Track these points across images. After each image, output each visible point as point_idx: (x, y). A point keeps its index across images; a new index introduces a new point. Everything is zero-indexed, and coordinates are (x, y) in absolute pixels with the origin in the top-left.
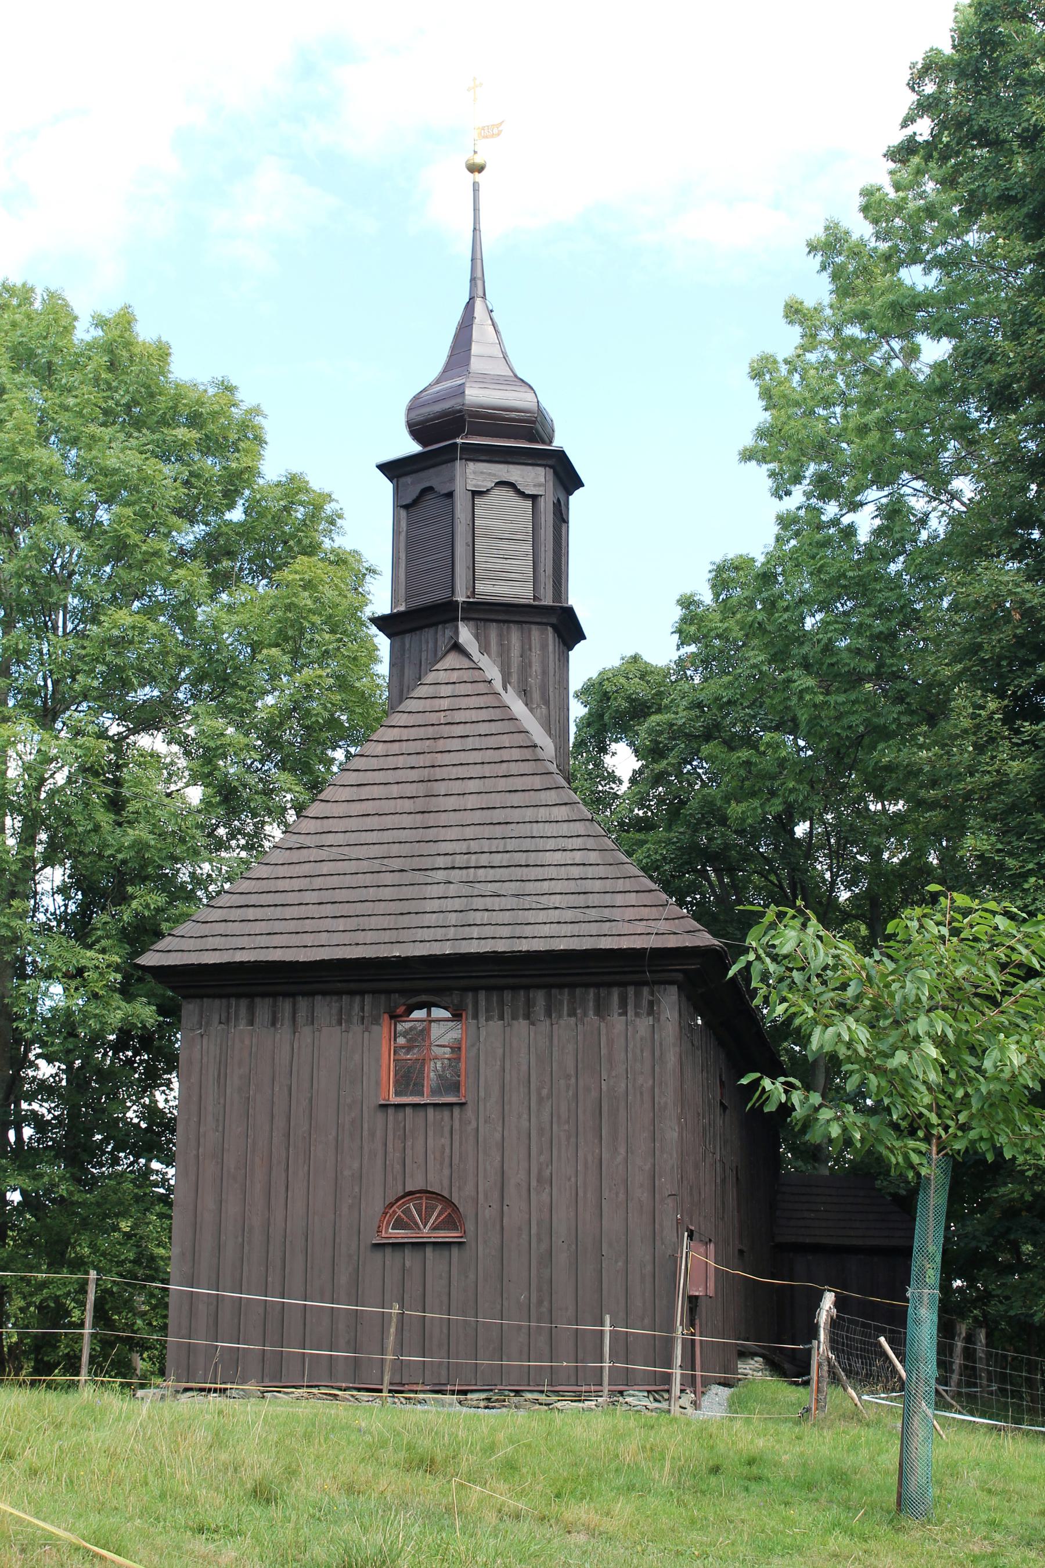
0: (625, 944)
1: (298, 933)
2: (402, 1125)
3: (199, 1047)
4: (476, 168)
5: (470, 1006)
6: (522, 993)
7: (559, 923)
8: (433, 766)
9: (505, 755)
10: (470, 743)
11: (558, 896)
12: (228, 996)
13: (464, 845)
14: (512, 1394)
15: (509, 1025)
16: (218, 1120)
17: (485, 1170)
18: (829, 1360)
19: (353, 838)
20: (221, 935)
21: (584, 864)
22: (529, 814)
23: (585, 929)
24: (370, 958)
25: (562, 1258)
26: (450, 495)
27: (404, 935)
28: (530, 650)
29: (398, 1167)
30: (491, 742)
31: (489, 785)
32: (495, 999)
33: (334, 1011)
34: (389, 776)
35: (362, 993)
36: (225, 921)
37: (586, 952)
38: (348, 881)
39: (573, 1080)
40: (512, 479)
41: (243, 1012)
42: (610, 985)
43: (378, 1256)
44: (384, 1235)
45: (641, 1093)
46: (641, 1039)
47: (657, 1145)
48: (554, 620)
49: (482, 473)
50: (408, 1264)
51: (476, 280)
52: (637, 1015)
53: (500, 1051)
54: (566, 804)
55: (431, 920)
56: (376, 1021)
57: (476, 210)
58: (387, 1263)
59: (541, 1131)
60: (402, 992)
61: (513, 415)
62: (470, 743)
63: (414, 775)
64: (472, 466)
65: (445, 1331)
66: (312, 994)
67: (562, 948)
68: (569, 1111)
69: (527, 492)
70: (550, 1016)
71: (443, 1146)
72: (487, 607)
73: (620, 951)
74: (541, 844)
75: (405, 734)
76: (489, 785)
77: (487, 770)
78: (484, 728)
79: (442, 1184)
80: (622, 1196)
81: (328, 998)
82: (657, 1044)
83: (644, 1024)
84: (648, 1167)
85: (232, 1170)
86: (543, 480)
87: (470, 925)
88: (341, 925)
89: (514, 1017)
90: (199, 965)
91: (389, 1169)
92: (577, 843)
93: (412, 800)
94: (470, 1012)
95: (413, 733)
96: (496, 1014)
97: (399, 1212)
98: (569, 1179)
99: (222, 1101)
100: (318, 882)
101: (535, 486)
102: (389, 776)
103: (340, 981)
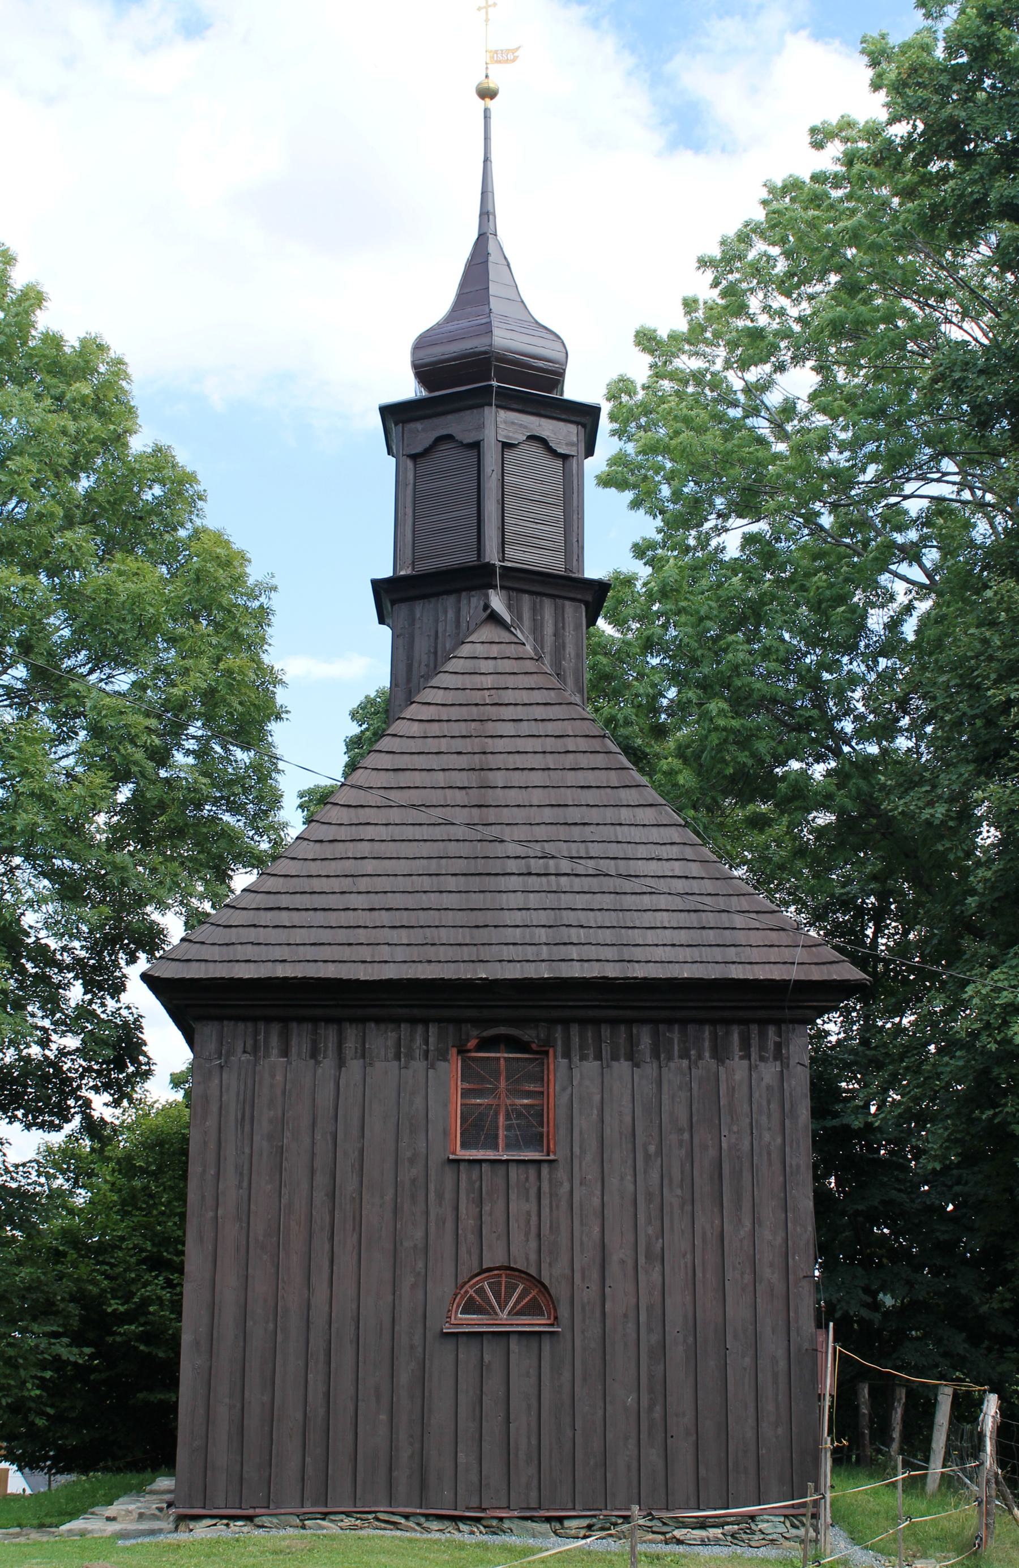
0: (761, 973)
1: (350, 944)
2: (477, 1184)
3: (217, 1081)
4: (487, 93)
5: (559, 1042)
6: (623, 1028)
7: (673, 945)
8: (484, 753)
9: (571, 744)
10: (525, 728)
11: (665, 914)
12: (255, 1019)
13: (538, 847)
14: (620, 1521)
15: (608, 1066)
16: (241, 1174)
17: (582, 1243)
18: (996, 1474)
19: (397, 832)
20: (252, 943)
21: (686, 877)
22: (610, 815)
23: (707, 954)
24: (450, 980)
25: (677, 1353)
26: (476, 446)
27: (485, 953)
28: (563, 628)
29: (471, 1237)
30: (550, 728)
31: (555, 777)
32: (590, 1034)
33: (390, 1043)
34: (434, 762)
35: (425, 1022)
36: (255, 926)
37: (797, 982)
38: (401, 883)
39: (686, 1136)
40: (544, 434)
41: (274, 1040)
42: (728, 1022)
43: (450, 1345)
44: (453, 1321)
45: (769, 1154)
46: (767, 1089)
47: (790, 1215)
48: (589, 598)
49: (513, 423)
50: (487, 1358)
51: (486, 214)
52: (762, 1059)
53: (597, 1098)
54: (651, 805)
55: (516, 935)
56: (443, 1056)
57: (487, 139)
58: (461, 1356)
59: (649, 1196)
60: (475, 1022)
61: (541, 364)
62: (525, 728)
63: (462, 762)
64: (503, 414)
65: (534, 1442)
66: (363, 1020)
67: (686, 976)
68: (682, 1172)
69: (560, 451)
70: (658, 1058)
71: (528, 1213)
74: (629, 851)
75: (445, 713)
76: (555, 777)
77: (551, 761)
78: (539, 712)
79: (527, 1259)
80: (748, 1278)
81: (383, 1026)
82: (787, 1094)
83: (769, 1071)
84: (779, 1240)
85: (261, 1238)
86: (575, 439)
87: (565, 944)
88: (403, 936)
89: (615, 1058)
90: (232, 979)
91: (461, 1239)
92: (674, 851)
93: (464, 792)
94: (559, 1049)
95: (455, 713)
96: (591, 1053)
97: (471, 1292)
98: (684, 1256)
99: (247, 1150)
100: (363, 884)
101: (567, 444)
102: (434, 762)
103: (401, 1006)
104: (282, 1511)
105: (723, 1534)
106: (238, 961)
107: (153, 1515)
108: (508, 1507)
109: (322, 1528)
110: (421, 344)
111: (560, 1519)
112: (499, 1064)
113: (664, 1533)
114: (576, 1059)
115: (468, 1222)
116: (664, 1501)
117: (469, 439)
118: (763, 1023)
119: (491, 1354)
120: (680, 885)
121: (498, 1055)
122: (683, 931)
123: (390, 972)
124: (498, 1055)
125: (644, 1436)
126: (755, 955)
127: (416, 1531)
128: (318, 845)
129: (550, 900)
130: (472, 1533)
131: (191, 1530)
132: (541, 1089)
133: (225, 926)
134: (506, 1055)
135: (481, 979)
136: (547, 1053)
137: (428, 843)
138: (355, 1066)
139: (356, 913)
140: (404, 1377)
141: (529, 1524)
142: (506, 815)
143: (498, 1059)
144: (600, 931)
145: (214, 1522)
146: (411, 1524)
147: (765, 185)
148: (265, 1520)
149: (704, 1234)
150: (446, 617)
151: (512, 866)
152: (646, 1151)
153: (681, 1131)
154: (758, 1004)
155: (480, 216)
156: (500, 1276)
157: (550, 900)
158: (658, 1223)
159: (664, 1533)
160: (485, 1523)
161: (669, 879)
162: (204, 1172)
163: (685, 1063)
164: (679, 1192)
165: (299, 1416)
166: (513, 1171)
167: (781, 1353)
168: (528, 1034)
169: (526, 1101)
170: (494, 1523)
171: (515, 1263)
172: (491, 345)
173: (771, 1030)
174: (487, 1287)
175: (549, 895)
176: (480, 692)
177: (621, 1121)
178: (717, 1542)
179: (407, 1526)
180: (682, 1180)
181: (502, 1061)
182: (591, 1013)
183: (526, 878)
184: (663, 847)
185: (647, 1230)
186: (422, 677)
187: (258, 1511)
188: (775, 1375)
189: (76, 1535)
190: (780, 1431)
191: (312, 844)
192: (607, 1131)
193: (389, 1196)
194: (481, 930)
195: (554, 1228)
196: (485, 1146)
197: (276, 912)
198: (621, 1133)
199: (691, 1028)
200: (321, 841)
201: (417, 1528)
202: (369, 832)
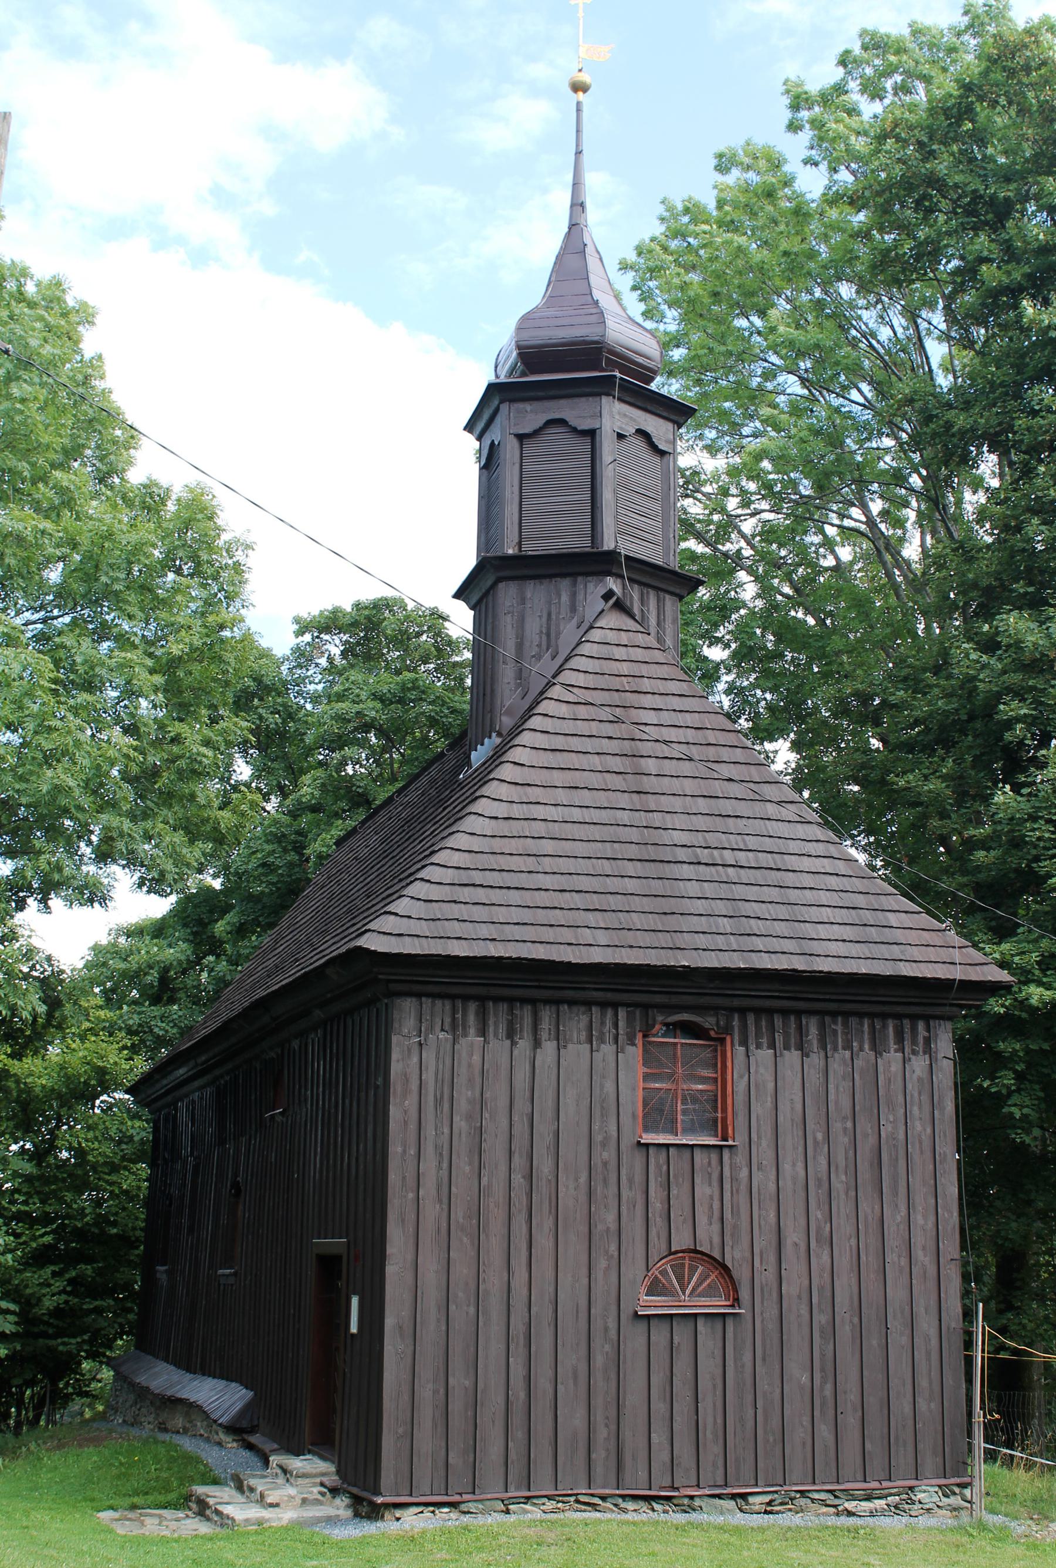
8: (633, 739)
14: (798, 1496)
20: (457, 920)
24: (655, 966)
25: (845, 1331)
26: (591, 434)
32: (764, 1023)
34: (588, 745)
35: (615, 1006)
39: (849, 1124)
40: (649, 429)
41: (472, 1019)
42: (884, 1016)
43: (642, 1326)
45: (920, 1143)
49: (625, 415)
53: (771, 1085)
57: (578, 131)
61: (640, 360)
65: (720, 1421)
67: (864, 971)
68: (846, 1159)
69: (661, 447)
70: (825, 1049)
71: (711, 1197)
72: (648, 569)
73: (925, 979)
79: (711, 1242)
81: (575, 1009)
83: (919, 1064)
89: (787, 1047)
90: (448, 956)
93: (620, 777)
96: (764, 1041)
102: (588, 745)
104: (489, 1496)
105: (888, 1505)
106: (449, 938)
107: (317, 1499)
108: (698, 1486)
109: (526, 1512)
110: (526, 322)
111: (744, 1496)
112: (675, 1049)
113: (835, 1506)
114: (752, 1047)
115: (657, 1205)
116: (835, 1474)
117: (584, 425)
118: (914, 1018)
119: (682, 1334)
120: (833, 882)
121: (676, 1040)
122: (848, 927)
123: (597, 956)
124: (676, 1040)
125: (817, 1413)
126: (916, 953)
127: (614, 1511)
128: (493, 821)
129: (723, 891)
130: (665, 1512)
131: (398, 1519)
132: (714, 1075)
133: (425, 901)
134: (683, 1041)
135: (684, 966)
136: (722, 1041)
137: (598, 826)
138: (549, 1047)
139: (548, 893)
140: (599, 1360)
141: (717, 1501)
142: (666, 802)
143: (675, 1044)
144: (775, 923)
145: (420, 1509)
146: (608, 1505)
147: (663, 202)
148: (472, 1507)
149: (866, 1218)
150: (560, 599)
151: (682, 854)
152: (815, 1139)
153: (845, 1118)
154: (917, 1000)
155: (572, 206)
156: (684, 1258)
157: (723, 891)
158: (827, 1207)
159: (835, 1506)
160: (675, 1501)
161: (822, 876)
162: (404, 1151)
163: (848, 1053)
164: (843, 1178)
165: (501, 1400)
166: (697, 1153)
167: (933, 1332)
168: (708, 1022)
169: (700, 1087)
170: (686, 1501)
171: (701, 1246)
172: (603, 336)
173: (921, 1026)
174: (670, 1270)
175: (721, 885)
176: (617, 678)
177: (792, 1109)
178: (883, 1513)
179: (605, 1507)
180: (846, 1166)
181: (679, 1046)
182: (768, 1003)
183: (696, 866)
184: (810, 844)
185: (817, 1214)
186: (533, 656)
187: (465, 1497)
188: (928, 1353)
189: (254, 1524)
190: (933, 1405)
191: (487, 820)
192: (781, 1119)
193: (583, 1178)
194: (669, 916)
195: (736, 1212)
196: (665, 1131)
197: (471, 889)
198: (792, 1120)
199: (853, 1021)
200: (496, 818)
201: (615, 1509)
202: (539, 812)
